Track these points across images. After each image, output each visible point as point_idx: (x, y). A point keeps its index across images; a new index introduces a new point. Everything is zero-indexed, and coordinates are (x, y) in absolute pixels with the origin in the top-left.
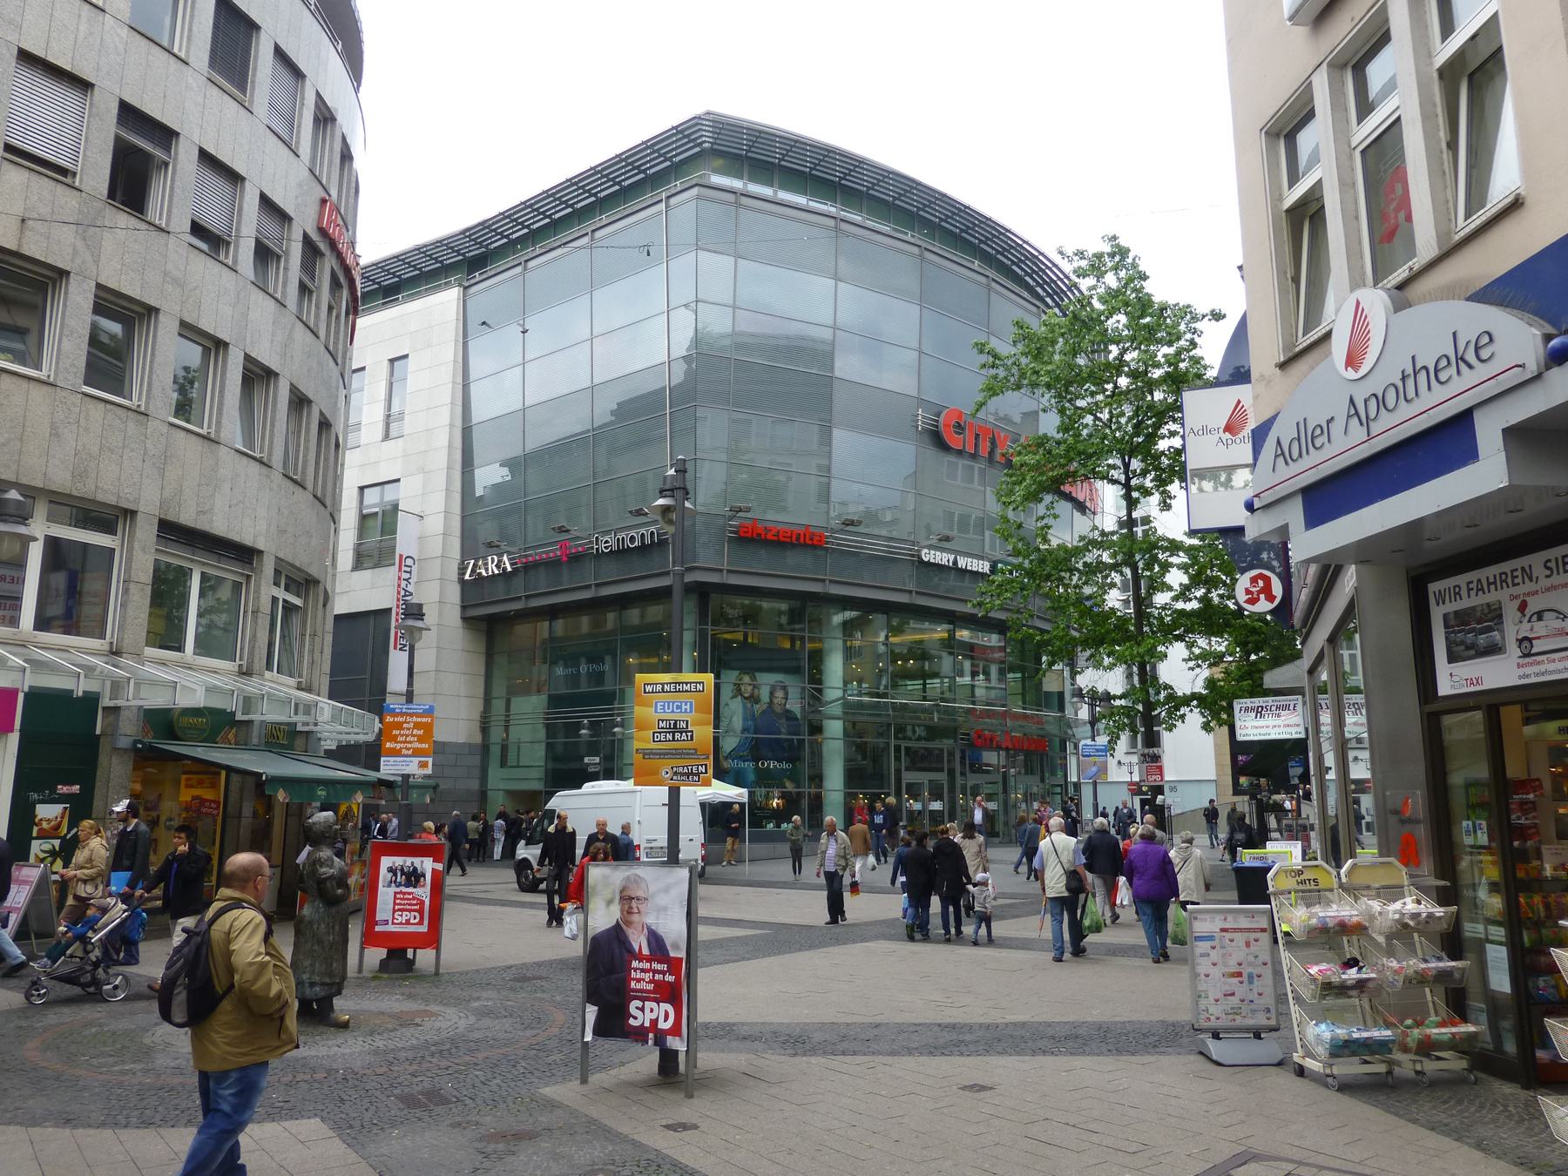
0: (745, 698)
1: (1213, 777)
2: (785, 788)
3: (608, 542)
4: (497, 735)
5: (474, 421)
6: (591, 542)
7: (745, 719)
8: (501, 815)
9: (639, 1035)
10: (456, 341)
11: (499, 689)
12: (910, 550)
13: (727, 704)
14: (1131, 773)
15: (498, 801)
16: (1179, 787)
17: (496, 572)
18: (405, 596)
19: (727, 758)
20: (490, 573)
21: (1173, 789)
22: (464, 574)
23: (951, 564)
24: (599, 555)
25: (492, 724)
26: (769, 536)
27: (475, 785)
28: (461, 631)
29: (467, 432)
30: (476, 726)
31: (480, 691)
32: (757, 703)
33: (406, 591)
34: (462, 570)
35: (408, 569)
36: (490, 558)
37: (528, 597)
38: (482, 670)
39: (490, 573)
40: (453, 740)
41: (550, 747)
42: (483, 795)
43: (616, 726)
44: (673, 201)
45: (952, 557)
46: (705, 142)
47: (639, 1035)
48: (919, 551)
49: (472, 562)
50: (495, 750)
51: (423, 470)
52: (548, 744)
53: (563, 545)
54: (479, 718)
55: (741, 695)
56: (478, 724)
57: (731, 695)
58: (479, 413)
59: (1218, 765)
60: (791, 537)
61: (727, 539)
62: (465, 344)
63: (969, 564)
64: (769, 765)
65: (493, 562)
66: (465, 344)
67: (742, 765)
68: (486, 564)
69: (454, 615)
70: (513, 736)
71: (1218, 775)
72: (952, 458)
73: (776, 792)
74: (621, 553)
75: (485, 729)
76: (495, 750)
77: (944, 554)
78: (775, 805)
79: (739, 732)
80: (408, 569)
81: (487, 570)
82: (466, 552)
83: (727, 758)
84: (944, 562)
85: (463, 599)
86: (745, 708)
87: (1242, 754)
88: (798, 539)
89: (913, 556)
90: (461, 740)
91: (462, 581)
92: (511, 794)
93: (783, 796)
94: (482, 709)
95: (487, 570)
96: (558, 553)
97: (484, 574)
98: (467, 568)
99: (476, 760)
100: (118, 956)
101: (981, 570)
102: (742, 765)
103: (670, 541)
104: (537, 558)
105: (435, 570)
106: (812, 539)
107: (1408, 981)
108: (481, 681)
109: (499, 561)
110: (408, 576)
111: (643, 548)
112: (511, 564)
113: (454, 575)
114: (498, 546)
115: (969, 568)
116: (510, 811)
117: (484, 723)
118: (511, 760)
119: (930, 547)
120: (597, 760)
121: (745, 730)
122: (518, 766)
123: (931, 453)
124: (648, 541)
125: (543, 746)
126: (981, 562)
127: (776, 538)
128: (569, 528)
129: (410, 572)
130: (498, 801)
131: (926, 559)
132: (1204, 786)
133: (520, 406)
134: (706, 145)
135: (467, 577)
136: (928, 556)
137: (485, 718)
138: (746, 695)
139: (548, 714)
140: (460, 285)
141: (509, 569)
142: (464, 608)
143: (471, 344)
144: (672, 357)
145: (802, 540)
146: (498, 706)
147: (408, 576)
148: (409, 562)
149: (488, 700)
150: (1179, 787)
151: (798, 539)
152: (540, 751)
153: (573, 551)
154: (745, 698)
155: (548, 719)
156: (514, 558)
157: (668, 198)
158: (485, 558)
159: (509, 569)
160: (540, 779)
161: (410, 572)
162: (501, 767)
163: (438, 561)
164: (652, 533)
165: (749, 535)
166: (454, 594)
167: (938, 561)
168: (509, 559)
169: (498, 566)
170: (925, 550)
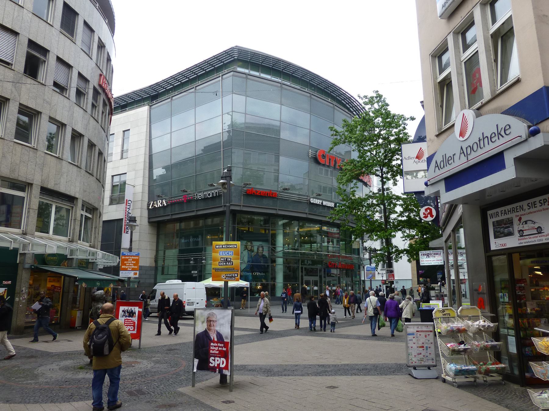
3: (200, 196)
4: (160, 263)
5: (153, 153)
6: (195, 196)
9: (213, 369)
11: (161, 247)
12: (307, 199)
14: (382, 277)
17: (161, 206)
18: (128, 214)
20: (159, 206)
21: (397, 282)
22: (149, 206)
29: (151, 156)
30: (153, 260)
31: (155, 248)
33: (128, 212)
34: (149, 205)
35: (129, 205)
36: (158, 201)
39: (159, 206)
41: (179, 267)
44: (224, 77)
45: (321, 201)
47: (213, 369)
48: (310, 199)
49: (152, 202)
50: (160, 269)
51: (135, 170)
52: (178, 266)
55: (247, 249)
58: (155, 150)
59: (413, 274)
60: (265, 194)
61: (242, 195)
62: (150, 126)
63: (327, 204)
66: (150, 126)
68: (157, 203)
71: (412, 277)
75: (156, 261)
76: (160, 269)
77: (318, 200)
78: (259, 288)
80: (129, 205)
81: (157, 205)
82: (150, 199)
84: (318, 203)
85: (149, 215)
86: (248, 254)
87: (421, 270)
88: (267, 195)
89: (307, 201)
91: (148, 209)
94: (155, 254)
95: (157, 205)
97: (156, 206)
98: (150, 204)
101: (331, 206)
103: (222, 195)
104: (175, 201)
105: (139, 205)
107: (481, 349)
108: (155, 244)
110: (129, 207)
111: (213, 198)
112: (166, 203)
113: (146, 207)
117: (156, 259)
119: (313, 198)
120: (196, 272)
121: (248, 262)
123: (314, 165)
124: (215, 195)
126: (331, 203)
131: (312, 202)
132: (408, 281)
133: (170, 147)
134: (236, 57)
135: (150, 207)
136: (313, 201)
137: (156, 257)
138: (249, 249)
139: (179, 256)
140: (148, 105)
141: (165, 205)
142: (149, 218)
145: (269, 195)
146: (161, 253)
148: (130, 202)
152: (176, 269)
154: (249, 250)
155: (179, 258)
157: (222, 75)
158: (157, 201)
159: (165, 205)
161: (130, 206)
162: (162, 274)
164: (216, 192)
167: (316, 202)
168: (165, 201)
170: (312, 199)
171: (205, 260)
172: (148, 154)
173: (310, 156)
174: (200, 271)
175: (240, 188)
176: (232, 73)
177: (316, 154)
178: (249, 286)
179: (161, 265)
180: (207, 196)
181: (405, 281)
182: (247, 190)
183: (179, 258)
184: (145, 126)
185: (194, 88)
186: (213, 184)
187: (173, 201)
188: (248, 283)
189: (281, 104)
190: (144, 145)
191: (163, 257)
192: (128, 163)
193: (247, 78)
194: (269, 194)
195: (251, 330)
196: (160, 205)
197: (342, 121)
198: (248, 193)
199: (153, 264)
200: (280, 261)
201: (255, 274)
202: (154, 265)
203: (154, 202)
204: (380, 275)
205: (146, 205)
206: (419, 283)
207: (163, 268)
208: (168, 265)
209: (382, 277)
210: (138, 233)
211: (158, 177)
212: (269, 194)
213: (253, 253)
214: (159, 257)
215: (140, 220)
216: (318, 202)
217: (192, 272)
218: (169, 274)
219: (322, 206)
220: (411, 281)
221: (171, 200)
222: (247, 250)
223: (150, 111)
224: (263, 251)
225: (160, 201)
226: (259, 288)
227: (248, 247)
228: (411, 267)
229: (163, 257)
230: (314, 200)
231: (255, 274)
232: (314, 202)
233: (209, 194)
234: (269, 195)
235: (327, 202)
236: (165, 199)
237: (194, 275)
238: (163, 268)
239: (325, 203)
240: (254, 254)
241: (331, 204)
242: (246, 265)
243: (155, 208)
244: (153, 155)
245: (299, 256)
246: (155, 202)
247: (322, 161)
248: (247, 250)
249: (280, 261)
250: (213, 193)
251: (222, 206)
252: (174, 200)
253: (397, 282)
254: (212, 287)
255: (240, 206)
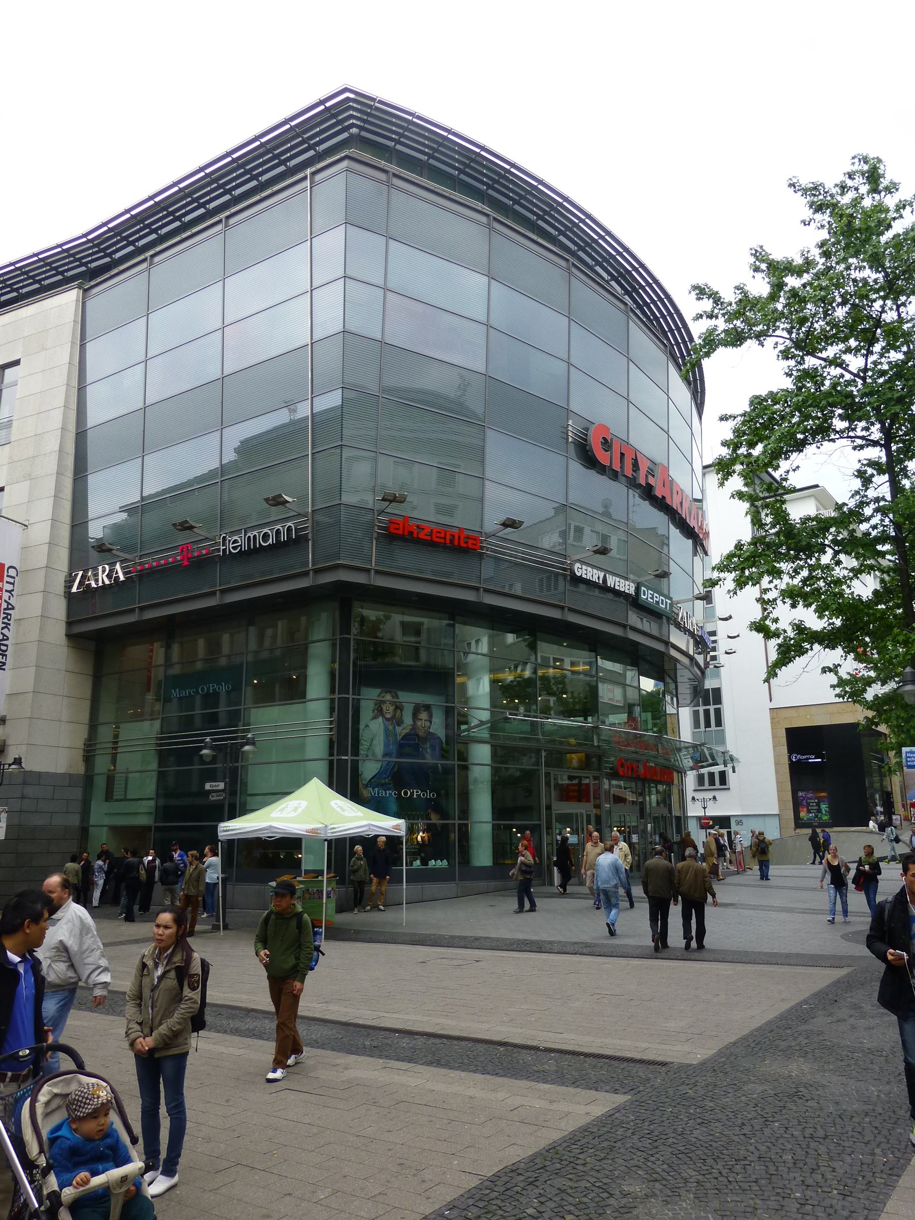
0: (387, 719)
1: (776, 812)
2: (430, 819)
3: (237, 542)
4: (102, 764)
5: (90, 424)
6: (218, 544)
7: (386, 745)
8: (104, 855)
10: (72, 342)
11: (107, 714)
12: (563, 563)
13: (367, 726)
14: (705, 808)
15: (101, 838)
16: (744, 820)
17: (107, 582)
18: (7, 609)
19: (367, 786)
20: (100, 584)
21: (739, 823)
22: (71, 587)
23: (601, 582)
24: (228, 558)
25: (98, 752)
26: (422, 536)
27: (74, 820)
28: (65, 649)
29: (81, 437)
30: (79, 755)
31: (85, 716)
32: (399, 725)
33: (8, 604)
34: (69, 582)
35: (11, 580)
36: (100, 568)
37: (142, 609)
38: (88, 694)
39: (100, 584)
40: (52, 770)
41: (161, 776)
42: (84, 831)
43: (247, 744)
44: (318, 177)
45: (602, 575)
46: (353, 125)
48: (572, 565)
49: (81, 573)
50: (100, 783)
51: (29, 477)
52: (159, 772)
53: (184, 548)
54: (83, 747)
55: (383, 716)
56: (81, 752)
57: (372, 715)
58: (94, 417)
59: (781, 801)
60: (445, 538)
61: (375, 535)
62: (83, 346)
63: (617, 584)
64: (412, 794)
65: (104, 571)
66: (83, 346)
67: (383, 793)
68: (96, 575)
69: (57, 632)
70: (121, 765)
71: (780, 810)
72: (592, 474)
73: (421, 824)
74: (252, 553)
75: (89, 757)
76: (100, 783)
77: (595, 571)
78: (419, 838)
79: (380, 756)
80: (11, 580)
81: (97, 581)
82: (73, 565)
83: (367, 786)
84: (595, 579)
85: (69, 615)
86: (386, 731)
87: (802, 791)
88: (452, 541)
89: (565, 569)
90: (61, 769)
91: (69, 595)
92: (115, 830)
93: (428, 829)
94: (86, 736)
95: (97, 581)
96: (179, 558)
97: (94, 585)
98: (74, 581)
99: (77, 793)
100: (153, 860)
102: (383, 793)
103: (310, 536)
104: (154, 564)
105: (38, 582)
106: (467, 542)
107: (341, 882)
108: (86, 705)
109: (111, 571)
110: (10, 587)
111: (279, 546)
112: (125, 573)
113: (60, 588)
114: (110, 550)
115: (617, 588)
116: (112, 847)
118: (118, 793)
119: (583, 563)
120: (221, 786)
121: (386, 755)
122: (125, 800)
123: (576, 467)
124: (284, 537)
125: (155, 774)
126: (627, 583)
127: (429, 538)
128: (193, 524)
129: (13, 584)
130: (101, 838)
131: (578, 574)
132: (767, 819)
133: (141, 405)
134: (354, 130)
135: (74, 590)
136: (582, 571)
137: (90, 745)
138: (388, 716)
139: (161, 739)
140: (79, 287)
141: (122, 578)
142: (69, 624)
143: (89, 346)
144: (315, 338)
145: (456, 543)
146: (105, 734)
147: (10, 587)
148: (12, 572)
149: (93, 726)
150: (744, 820)
151: (452, 541)
152: (150, 788)
153: (196, 554)
154: (387, 719)
155: (161, 745)
156: (127, 567)
157: (314, 174)
158: (95, 569)
159: (122, 578)
160: (151, 813)
161: (13, 584)
162: (107, 800)
163: (43, 572)
164: (289, 529)
165: (400, 532)
166: (59, 609)
167: (589, 577)
168: (122, 568)
169: (109, 576)
170: (577, 565)
171: (253, 744)
172: (74, 430)
173: (570, 440)
174: (232, 790)
175: (369, 517)
176: (345, 163)
177: (586, 435)
178: (403, 833)
179: (106, 771)
180: (260, 540)
181: (762, 819)
182: (391, 522)
183: (161, 745)
184: (68, 347)
185: (220, 221)
186: (280, 496)
187: (146, 566)
188: (401, 822)
189: (491, 278)
190: (60, 401)
191: (111, 745)
192: (11, 457)
193: (390, 185)
194: (457, 537)
195: (550, 1065)
196: (103, 579)
197: (748, 252)
198: (392, 530)
199: (80, 768)
200: (482, 753)
201: (406, 793)
202: (80, 769)
203: (86, 571)
204: (699, 804)
205: (63, 584)
206: (799, 824)
207: (110, 780)
208: (127, 769)
209: (705, 808)
210: (33, 669)
211: (107, 530)
212: (457, 537)
213: (398, 729)
214: (98, 746)
215: (41, 629)
216: (594, 575)
217: (208, 786)
218: (129, 797)
219: (604, 588)
220: (776, 821)
221: (141, 564)
222: (380, 720)
223: (84, 303)
224: (431, 722)
225: (107, 567)
226: (419, 838)
227: (384, 707)
228: (778, 782)
229: (111, 745)
230: (584, 567)
231: (406, 793)
232: (584, 576)
233: (266, 537)
234: (456, 543)
235: (618, 579)
236: (122, 562)
237: (214, 798)
238: (110, 780)
239: (611, 581)
240: (405, 732)
241: (627, 587)
242: (378, 765)
243: (87, 591)
244: (89, 433)
245: (538, 740)
246: (90, 574)
247: (602, 457)
248: (380, 720)
249: (482, 753)
250: (278, 532)
251: (306, 574)
252: (150, 562)
253: (739, 823)
254: (278, 836)
255: (368, 571)
